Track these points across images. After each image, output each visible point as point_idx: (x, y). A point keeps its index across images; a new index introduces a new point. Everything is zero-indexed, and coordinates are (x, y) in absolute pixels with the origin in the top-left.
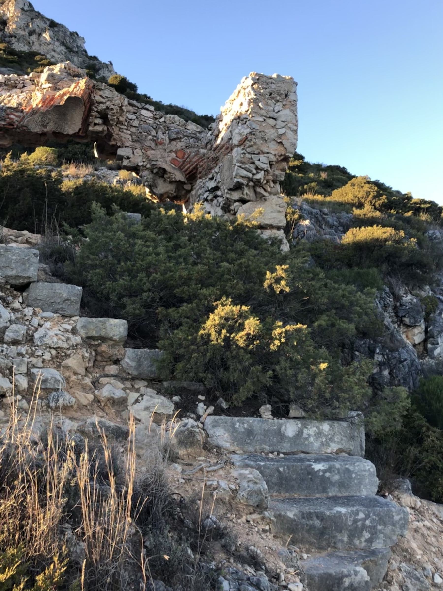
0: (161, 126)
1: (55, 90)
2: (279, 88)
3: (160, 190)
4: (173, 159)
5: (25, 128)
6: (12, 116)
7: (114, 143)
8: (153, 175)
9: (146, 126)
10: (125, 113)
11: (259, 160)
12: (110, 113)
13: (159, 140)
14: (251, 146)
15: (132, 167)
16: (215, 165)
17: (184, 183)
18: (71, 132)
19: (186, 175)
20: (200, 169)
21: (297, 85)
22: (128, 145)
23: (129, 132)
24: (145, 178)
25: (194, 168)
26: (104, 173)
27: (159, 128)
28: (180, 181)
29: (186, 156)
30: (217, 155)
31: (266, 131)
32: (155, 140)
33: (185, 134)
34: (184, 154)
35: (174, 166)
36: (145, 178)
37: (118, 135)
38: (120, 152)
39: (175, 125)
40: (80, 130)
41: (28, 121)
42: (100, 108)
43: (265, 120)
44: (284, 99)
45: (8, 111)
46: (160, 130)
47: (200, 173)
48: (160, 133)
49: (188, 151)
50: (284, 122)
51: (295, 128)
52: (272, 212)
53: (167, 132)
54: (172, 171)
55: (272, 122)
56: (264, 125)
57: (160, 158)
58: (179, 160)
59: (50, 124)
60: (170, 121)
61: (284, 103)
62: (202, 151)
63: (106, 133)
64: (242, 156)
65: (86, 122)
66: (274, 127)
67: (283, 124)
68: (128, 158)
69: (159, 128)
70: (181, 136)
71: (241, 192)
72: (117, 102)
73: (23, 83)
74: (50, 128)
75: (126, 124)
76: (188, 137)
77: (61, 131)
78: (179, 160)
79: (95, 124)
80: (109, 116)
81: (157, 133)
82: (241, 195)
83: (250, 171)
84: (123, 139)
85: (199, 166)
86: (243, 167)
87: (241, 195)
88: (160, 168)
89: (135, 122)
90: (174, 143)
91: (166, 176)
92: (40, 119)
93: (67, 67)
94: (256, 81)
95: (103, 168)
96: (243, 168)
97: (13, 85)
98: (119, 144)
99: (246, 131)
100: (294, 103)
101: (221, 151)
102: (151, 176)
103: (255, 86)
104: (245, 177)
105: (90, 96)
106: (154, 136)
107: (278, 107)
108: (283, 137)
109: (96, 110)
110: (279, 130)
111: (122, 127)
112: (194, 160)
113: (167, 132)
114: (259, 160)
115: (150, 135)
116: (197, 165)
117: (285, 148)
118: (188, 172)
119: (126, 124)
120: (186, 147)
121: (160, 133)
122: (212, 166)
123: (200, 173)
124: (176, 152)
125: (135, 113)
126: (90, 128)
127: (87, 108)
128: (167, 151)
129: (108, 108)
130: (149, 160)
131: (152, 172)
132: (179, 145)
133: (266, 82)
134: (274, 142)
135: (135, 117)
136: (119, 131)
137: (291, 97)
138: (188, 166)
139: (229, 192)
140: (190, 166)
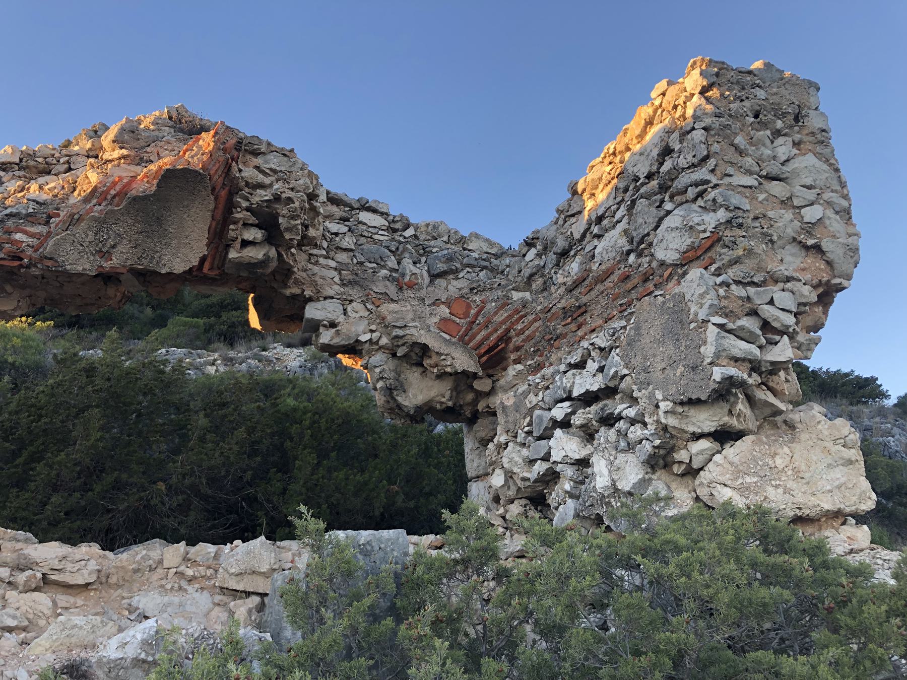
0: (409, 246)
1: (139, 164)
2: (776, 99)
3: (415, 396)
4: (444, 320)
5: (50, 263)
6: (18, 236)
7: (296, 290)
8: (396, 361)
9: (373, 247)
10: (320, 219)
11: (771, 302)
12: (285, 212)
13: (407, 279)
14: (736, 261)
15: (344, 346)
16: (573, 327)
17: (475, 376)
18: (179, 267)
19: (480, 357)
20: (516, 341)
21: (818, 89)
22: (330, 292)
23: (333, 264)
24: (378, 370)
25: (500, 339)
26: (278, 353)
27: (405, 250)
28: (464, 372)
29: (473, 312)
30: (584, 300)
31: (771, 214)
32: (394, 279)
33: (465, 261)
34: (469, 307)
35: (448, 337)
36: (378, 370)
37: (305, 270)
38: (312, 312)
39: (438, 243)
40: (203, 260)
41: (56, 244)
42: (255, 199)
43: (760, 184)
44: (791, 127)
45: (10, 223)
46: (407, 255)
47: (517, 349)
48: (407, 263)
49: (478, 299)
50: (809, 187)
51: (845, 203)
52: (829, 466)
53: (423, 259)
54: (444, 349)
55: (776, 188)
56: (761, 197)
57: (413, 320)
58: (458, 320)
59: (120, 248)
60: (428, 233)
61: (797, 137)
62: (516, 296)
63: (274, 264)
64: (722, 292)
65: (219, 238)
66: (786, 203)
67: (811, 195)
68: (333, 325)
69: (405, 250)
70: (458, 266)
71: (726, 407)
72: (301, 182)
73: (68, 162)
74: (120, 258)
75: (325, 244)
76: (471, 266)
77: (153, 266)
78: (458, 320)
79: (245, 244)
80: (281, 220)
81: (399, 263)
82: (726, 419)
83: (749, 338)
84: (320, 281)
85: (513, 333)
86: (731, 326)
87: (726, 419)
88: (415, 344)
89: (347, 239)
90: (441, 282)
91: (427, 362)
92: (91, 237)
93: (174, 115)
94: (714, 79)
95: (276, 345)
96: (729, 331)
97: (41, 167)
98: (308, 293)
99: (711, 220)
100: (822, 138)
101: (600, 287)
102: (391, 364)
103: (714, 93)
104: (744, 360)
105: (229, 168)
106: (393, 270)
107: (783, 148)
108: (818, 232)
109: (245, 204)
110: (803, 211)
111: (315, 251)
112: (499, 318)
113: (423, 259)
114: (771, 302)
115: (384, 267)
116: (508, 331)
117: (829, 263)
118: (483, 350)
119: (325, 244)
120: (472, 289)
121: (407, 263)
122: (560, 329)
123: (517, 349)
124: (448, 304)
125: (344, 220)
126: (233, 255)
127: (222, 200)
128: (427, 302)
129: (277, 198)
130: (386, 327)
131: (394, 355)
132: (455, 286)
133: (738, 83)
134: (793, 249)
135: (345, 229)
136: (309, 261)
137: (814, 122)
138: (483, 333)
139: (680, 409)
140: (491, 334)
